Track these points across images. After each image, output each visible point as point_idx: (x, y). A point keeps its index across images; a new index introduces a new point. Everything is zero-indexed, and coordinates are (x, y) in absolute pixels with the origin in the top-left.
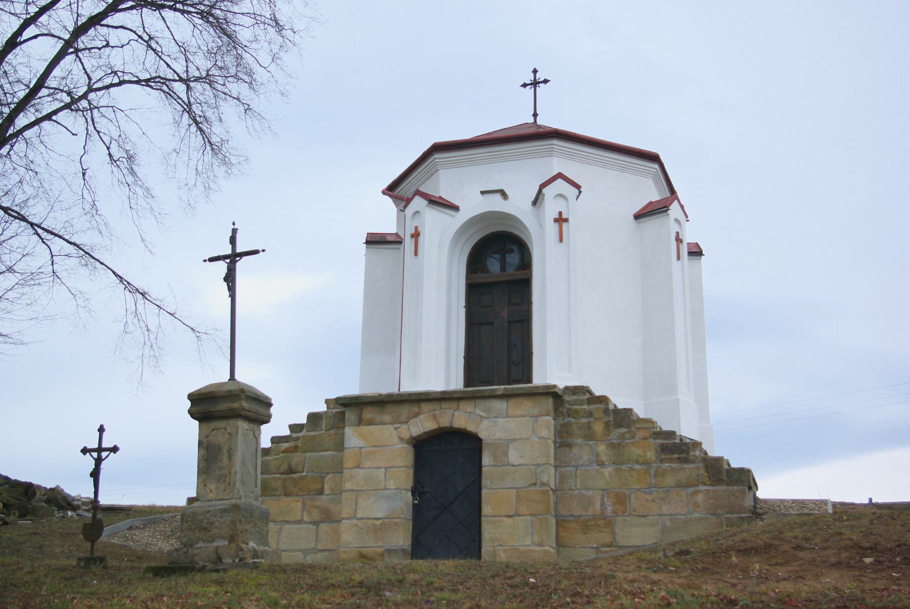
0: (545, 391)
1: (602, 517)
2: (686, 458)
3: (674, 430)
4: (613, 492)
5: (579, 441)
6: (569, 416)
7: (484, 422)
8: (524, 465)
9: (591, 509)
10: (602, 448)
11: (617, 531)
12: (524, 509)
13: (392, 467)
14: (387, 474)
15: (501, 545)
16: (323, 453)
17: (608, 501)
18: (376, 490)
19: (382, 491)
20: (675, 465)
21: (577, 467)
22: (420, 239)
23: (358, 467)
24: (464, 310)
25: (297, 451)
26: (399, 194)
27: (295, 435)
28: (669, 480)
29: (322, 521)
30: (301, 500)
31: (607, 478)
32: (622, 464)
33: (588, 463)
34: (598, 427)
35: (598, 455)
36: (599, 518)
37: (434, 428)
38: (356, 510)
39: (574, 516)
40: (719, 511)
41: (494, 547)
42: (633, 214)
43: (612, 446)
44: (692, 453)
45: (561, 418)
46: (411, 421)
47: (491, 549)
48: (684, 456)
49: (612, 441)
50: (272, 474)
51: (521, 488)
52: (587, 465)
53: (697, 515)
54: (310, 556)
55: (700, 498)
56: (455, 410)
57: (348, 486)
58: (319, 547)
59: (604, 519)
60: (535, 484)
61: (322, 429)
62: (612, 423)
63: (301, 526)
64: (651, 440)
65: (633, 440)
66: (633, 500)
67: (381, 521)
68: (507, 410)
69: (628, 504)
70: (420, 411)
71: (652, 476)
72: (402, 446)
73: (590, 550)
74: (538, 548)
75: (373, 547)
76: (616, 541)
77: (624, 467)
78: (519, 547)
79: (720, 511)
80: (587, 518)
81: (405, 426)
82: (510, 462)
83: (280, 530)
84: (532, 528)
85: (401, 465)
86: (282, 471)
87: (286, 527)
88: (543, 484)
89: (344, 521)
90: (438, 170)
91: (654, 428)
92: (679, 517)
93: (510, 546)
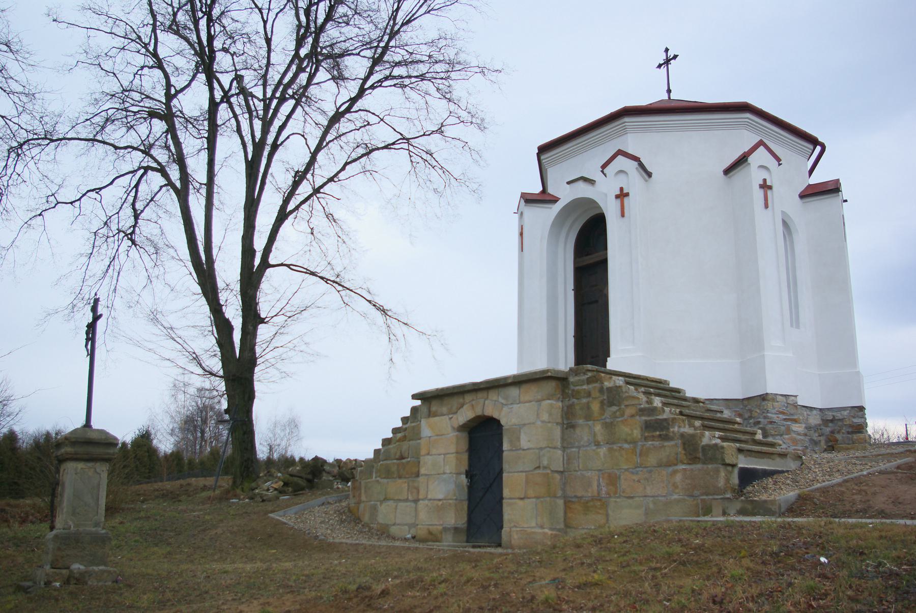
0: (542, 376)
1: (599, 498)
2: (667, 435)
3: (373, 451)
5: (581, 422)
7: (504, 409)
10: (598, 428)
11: (610, 512)
12: (531, 493)
15: (515, 526)
18: (439, 474)
20: (657, 443)
21: (579, 447)
23: (428, 454)
24: (573, 292)
28: (652, 460)
32: (613, 443)
34: (595, 407)
35: (595, 435)
40: (696, 493)
42: (723, 169)
44: (672, 430)
45: (567, 400)
48: (664, 432)
50: (392, 460)
52: (587, 446)
53: (676, 497)
55: (678, 478)
56: (485, 400)
59: (600, 500)
60: (539, 467)
62: (605, 402)
64: (638, 417)
68: (519, 396)
69: (618, 485)
71: (638, 455)
74: (540, 531)
77: (615, 447)
79: (696, 492)
86: (397, 457)
88: (545, 468)
89: (421, 502)
91: (641, 405)
92: (660, 498)
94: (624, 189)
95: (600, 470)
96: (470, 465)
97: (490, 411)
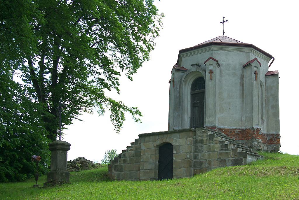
23: (144, 155)
57: (142, 160)
60: (186, 158)
66: (213, 162)
96: (159, 158)
97: (168, 141)
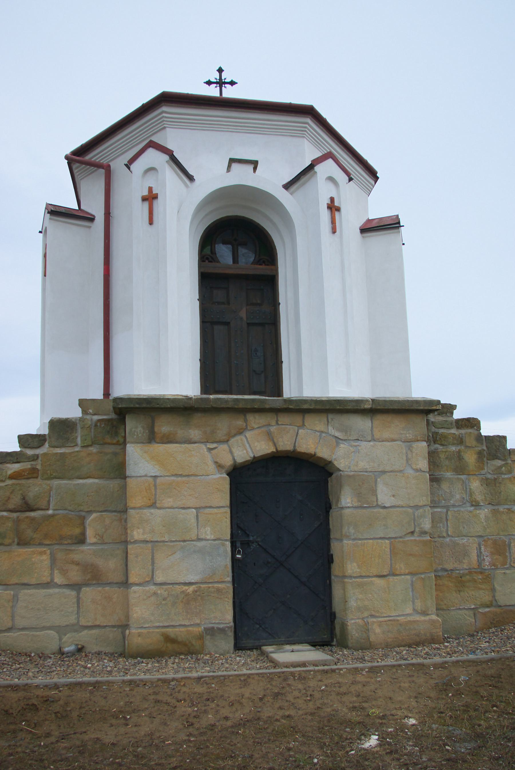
1: (479, 570)
4: (492, 539)
5: (449, 474)
6: (435, 443)
7: (342, 445)
8: (398, 507)
9: (466, 561)
10: (475, 484)
12: (400, 567)
13: (206, 507)
14: (200, 519)
15: (372, 616)
16: (81, 481)
17: (485, 551)
18: (184, 541)
19: (194, 543)
22: (158, 205)
23: (153, 505)
25: (37, 477)
26: (93, 160)
27: (30, 452)
29: (87, 584)
30: (48, 552)
31: (483, 523)
32: (499, 504)
33: (461, 504)
35: (471, 494)
36: (475, 572)
37: (269, 451)
38: (153, 572)
39: (446, 570)
41: (363, 619)
43: (487, 482)
46: (232, 441)
47: (360, 621)
49: (486, 476)
51: (395, 538)
54: (68, 635)
57: (137, 534)
58: (83, 622)
59: (481, 573)
60: (412, 533)
61: (77, 445)
63: (51, 591)
65: (510, 476)
67: (194, 586)
70: (246, 426)
72: (220, 475)
73: (467, 612)
74: (423, 618)
75: (184, 626)
76: (496, 600)
77: (501, 509)
78: (399, 618)
80: (461, 572)
81: (224, 447)
82: (379, 503)
83: (15, 598)
84: (413, 591)
85: (221, 505)
86: (11, 506)
87: (25, 594)
90: (165, 128)
93: (386, 617)
94: (153, 189)
95: (481, 536)
